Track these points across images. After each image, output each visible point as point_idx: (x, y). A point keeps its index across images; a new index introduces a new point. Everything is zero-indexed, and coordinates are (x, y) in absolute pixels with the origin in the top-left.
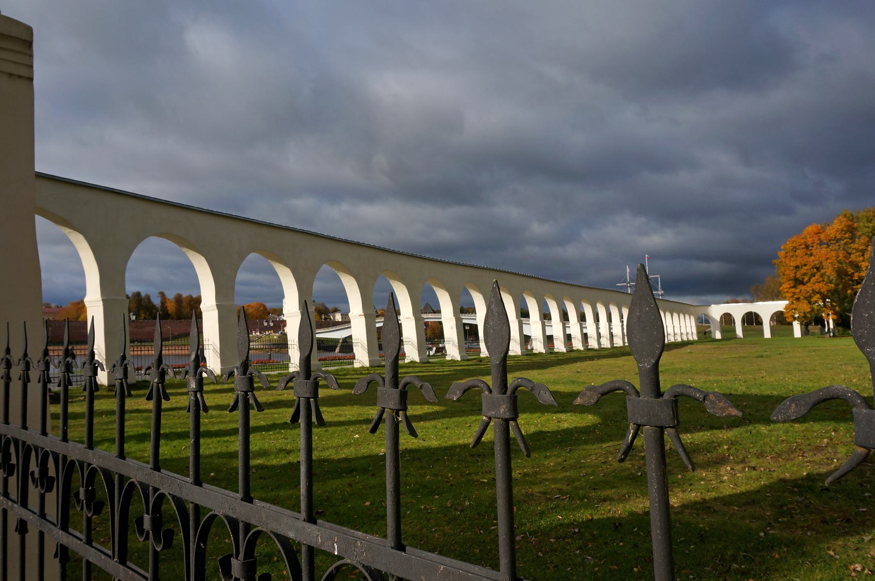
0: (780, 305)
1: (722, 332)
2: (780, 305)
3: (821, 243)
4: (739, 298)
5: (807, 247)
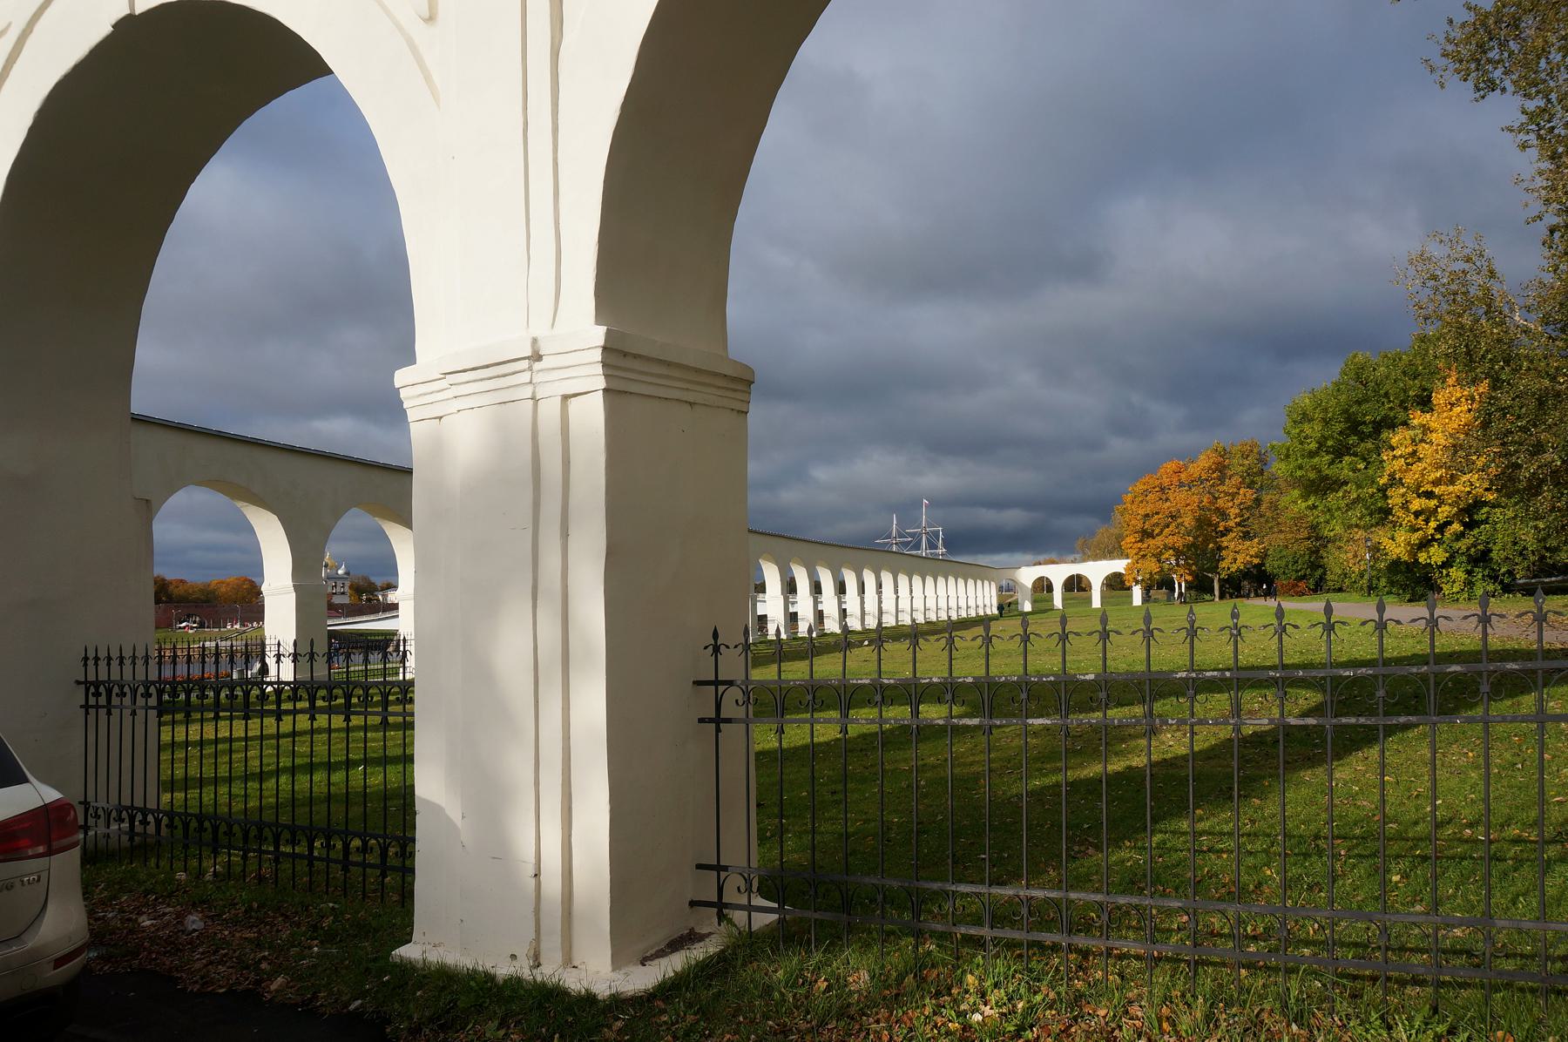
0: (1119, 565)
1: (1034, 602)
2: (1119, 565)
3: (1181, 485)
4: (1041, 558)
5: (1162, 490)
